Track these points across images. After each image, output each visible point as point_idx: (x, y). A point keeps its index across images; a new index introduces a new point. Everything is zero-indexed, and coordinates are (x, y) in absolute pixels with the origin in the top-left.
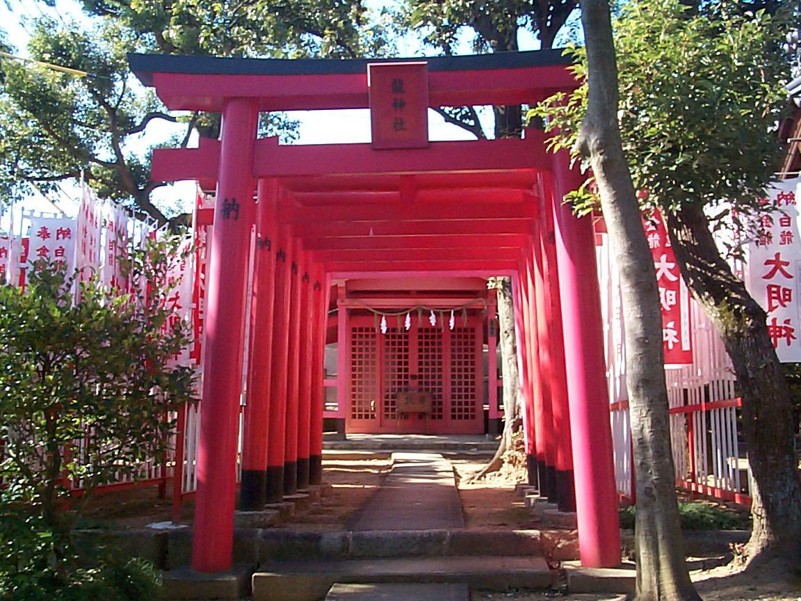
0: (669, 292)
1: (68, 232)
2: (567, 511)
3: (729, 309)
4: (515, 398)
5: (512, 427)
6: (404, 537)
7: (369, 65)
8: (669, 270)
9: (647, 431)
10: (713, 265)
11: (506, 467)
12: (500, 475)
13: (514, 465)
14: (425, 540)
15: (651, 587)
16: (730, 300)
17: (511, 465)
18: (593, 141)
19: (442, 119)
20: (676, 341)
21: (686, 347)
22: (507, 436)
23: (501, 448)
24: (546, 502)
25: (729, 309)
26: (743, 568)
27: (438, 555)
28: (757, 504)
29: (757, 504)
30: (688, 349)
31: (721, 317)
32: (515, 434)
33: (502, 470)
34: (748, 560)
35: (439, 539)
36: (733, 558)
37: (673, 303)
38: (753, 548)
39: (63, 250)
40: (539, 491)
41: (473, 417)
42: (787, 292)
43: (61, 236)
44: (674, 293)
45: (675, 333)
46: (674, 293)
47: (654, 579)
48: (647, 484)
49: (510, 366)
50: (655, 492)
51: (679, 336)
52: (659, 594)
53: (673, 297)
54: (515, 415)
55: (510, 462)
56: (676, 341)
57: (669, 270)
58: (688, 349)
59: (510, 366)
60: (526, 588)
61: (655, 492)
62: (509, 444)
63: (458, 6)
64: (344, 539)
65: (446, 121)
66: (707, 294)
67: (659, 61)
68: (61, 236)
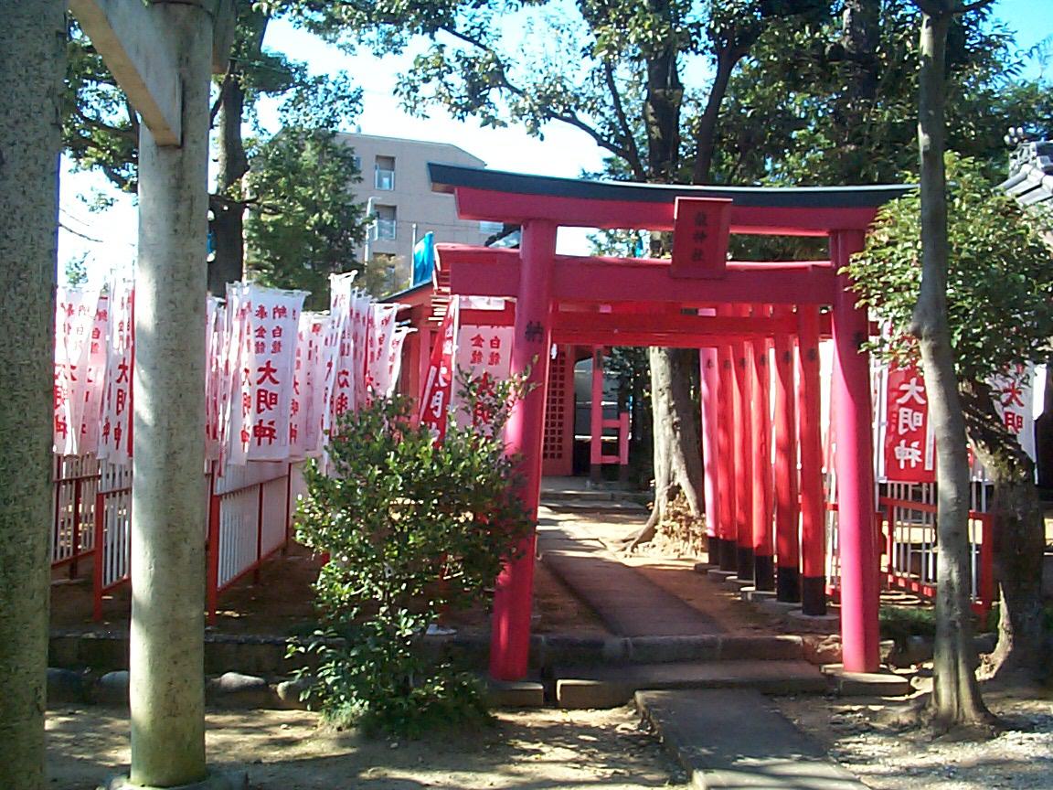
0: (916, 414)
1: (284, 310)
2: (814, 614)
3: (1003, 460)
4: (670, 464)
5: (668, 495)
6: (681, 643)
7: (677, 198)
8: (918, 392)
9: (955, 575)
10: (989, 417)
11: (659, 538)
12: (654, 546)
13: (669, 536)
14: (699, 646)
15: (952, 700)
16: (1005, 450)
17: (666, 536)
18: (926, 328)
19: (593, 141)
20: (919, 460)
21: (929, 467)
22: (661, 503)
23: (652, 516)
24: (774, 600)
25: (1003, 460)
26: (991, 675)
27: (711, 660)
28: (1003, 620)
29: (1003, 620)
30: (931, 469)
31: (995, 465)
32: (671, 503)
33: (654, 541)
34: (996, 668)
35: (711, 645)
36: (980, 665)
37: (920, 424)
38: (998, 656)
39: (281, 330)
40: (754, 582)
41: (560, 456)
42: (1010, 416)
43: (277, 315)
44: (921, 415)
45: (919, 453)
46: (921, 415)
47: (955, 695)
48: (952, 619)
49: (664, 428)
50: (958, 624)
51: (922, 456)
52: (958, 706)
53: (921, 419)
54: (669, 482)
55: (665, 533)
56: (919, 460)
57: (918, 392)
58: (931, 469)
59: (664, 428)
60: (804, 692)
61: (958, 624)
62: (663, 513)
63: (646, 37)
64: (626, 645)
65: (599, 145)
66: (983, 443)
67: (908, 179)
68: (277, 315)
